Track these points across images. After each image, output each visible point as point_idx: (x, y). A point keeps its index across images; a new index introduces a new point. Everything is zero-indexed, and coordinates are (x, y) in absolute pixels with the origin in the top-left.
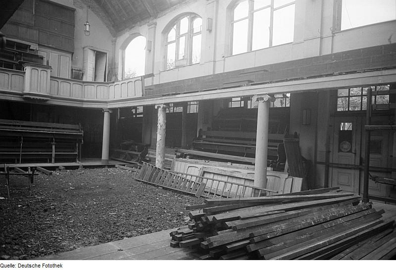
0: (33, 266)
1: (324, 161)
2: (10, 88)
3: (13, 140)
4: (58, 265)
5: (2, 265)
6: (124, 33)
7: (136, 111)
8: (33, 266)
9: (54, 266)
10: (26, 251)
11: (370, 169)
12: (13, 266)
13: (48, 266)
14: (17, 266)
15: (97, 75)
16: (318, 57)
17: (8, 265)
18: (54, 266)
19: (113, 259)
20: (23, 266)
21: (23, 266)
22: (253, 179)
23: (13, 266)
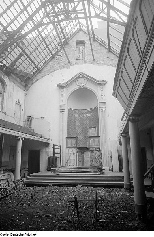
0: (20, 235)
1: (91, 15)
2: (64, 110)
3: (137, 3)
4: (34, 234)
5: (1, 234)
6: (140, 191)
7: (64, 11)
8: (20, 235)
9: (31, 234)
10: (10, 66)
11: (83, 11)
12: (8, 235)
13: (28, 235)
14: (10, 235)
16: (126, 28)
17: (5, 234)
18: (31, 234)
19: (72, 231)
20: (13, 235)
21: (13, 235)
22: (104, 101)
23: (8, 235)
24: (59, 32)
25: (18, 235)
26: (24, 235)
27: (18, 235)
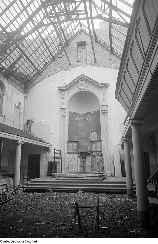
0: (20, 242)
4: (35, 241)
5: (1, 241)
8: (20, 242)
9: (32, 241)
12: (8, 242)
13: (29, 241)
14: (10, 242)
15: (146, 14)
17: (5, 241)
18: (32, 241)
20: (14, 242)
21: (14, 242)
23: (8, 242)
24: (60, 33)
25: (18, 242)
26: (25, 242)
27: (18, 242)
